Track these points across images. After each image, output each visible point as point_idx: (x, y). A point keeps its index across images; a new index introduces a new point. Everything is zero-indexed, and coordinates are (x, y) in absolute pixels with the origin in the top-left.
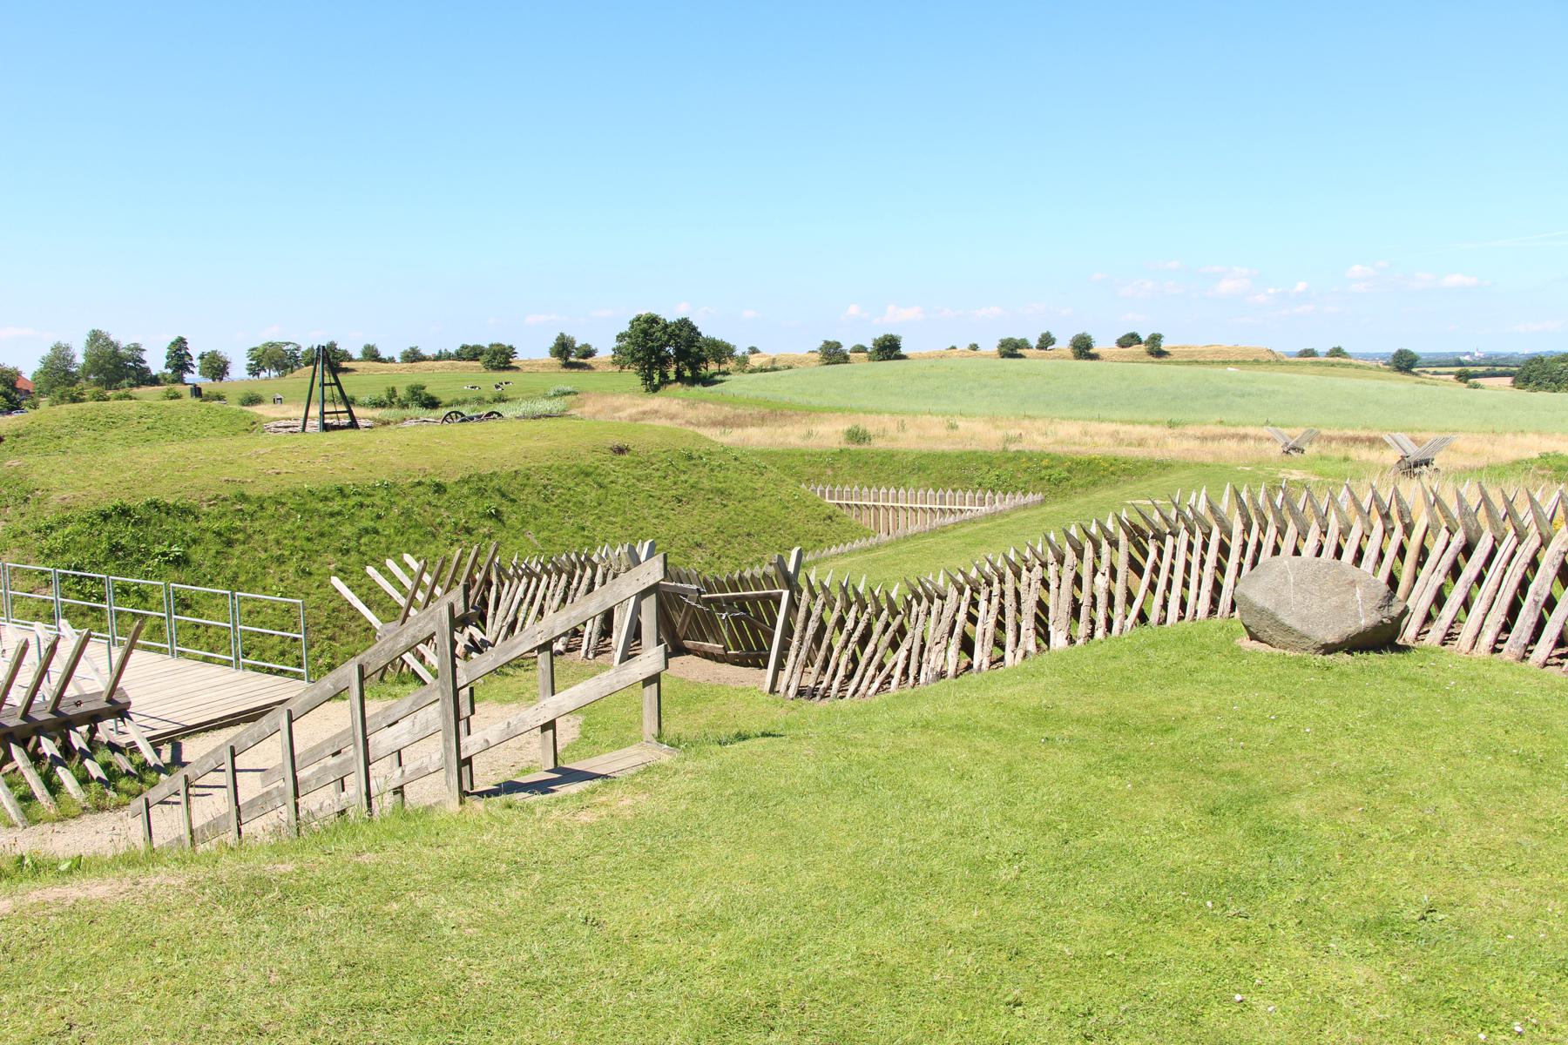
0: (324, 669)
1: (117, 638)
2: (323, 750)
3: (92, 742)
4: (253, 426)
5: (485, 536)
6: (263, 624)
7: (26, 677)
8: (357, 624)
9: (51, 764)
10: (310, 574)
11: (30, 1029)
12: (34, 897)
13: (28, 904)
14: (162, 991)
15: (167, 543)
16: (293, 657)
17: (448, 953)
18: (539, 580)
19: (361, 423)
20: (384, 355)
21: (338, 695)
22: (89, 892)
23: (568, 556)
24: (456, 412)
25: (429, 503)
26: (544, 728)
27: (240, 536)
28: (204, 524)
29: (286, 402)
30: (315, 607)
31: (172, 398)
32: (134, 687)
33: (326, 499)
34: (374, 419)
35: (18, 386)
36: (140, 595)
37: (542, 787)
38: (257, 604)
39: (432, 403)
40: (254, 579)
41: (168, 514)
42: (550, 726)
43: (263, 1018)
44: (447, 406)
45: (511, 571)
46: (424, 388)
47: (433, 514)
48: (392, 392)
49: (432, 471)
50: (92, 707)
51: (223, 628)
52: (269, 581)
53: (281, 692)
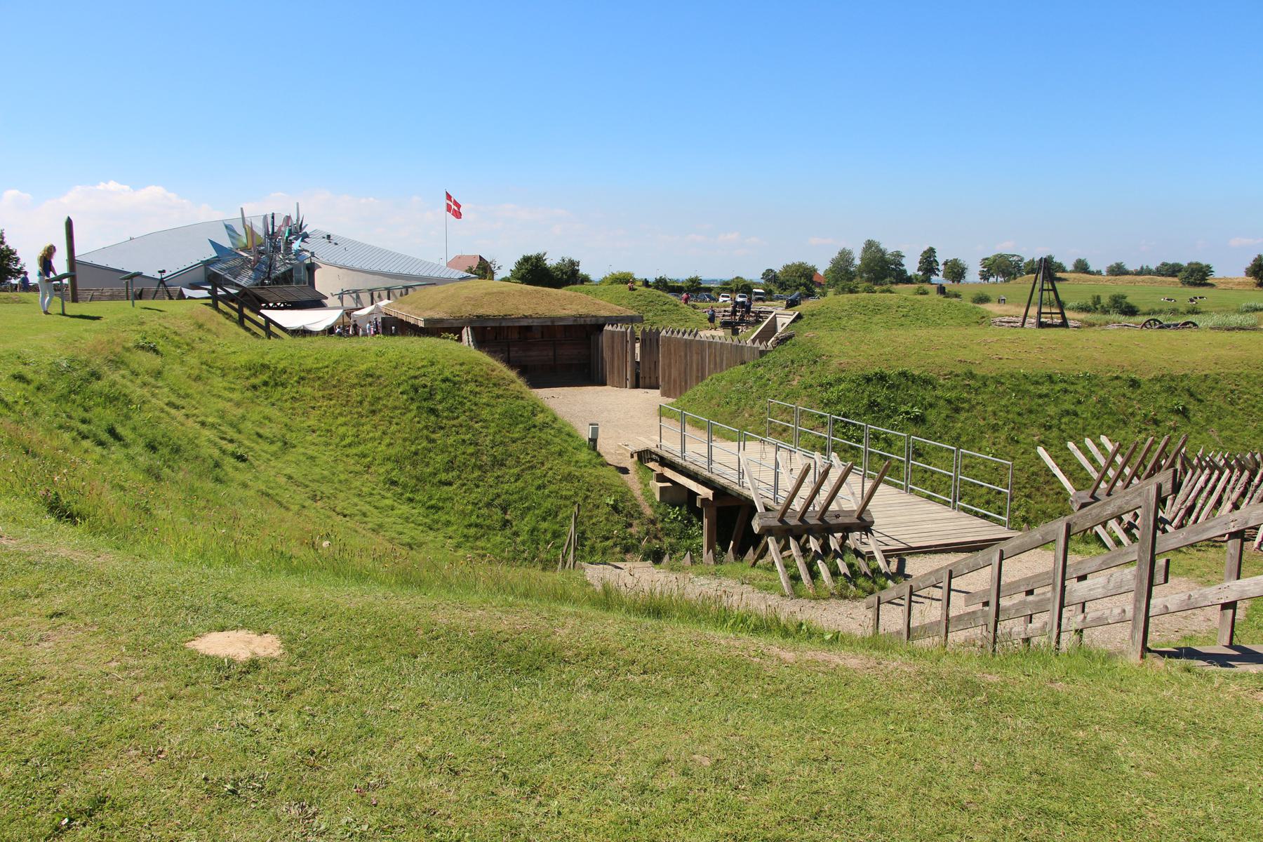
0: (1019, 520)
1: (868, 471)
2: (1019, 587)
3: (842, 546)
4: (983, 320)
5: (1170, 428)
6: (975, 477)
7: (805, 491)
8: (1051, 487)
9: (814, 556)
10: (1017, 442)
11: (801, 751)
12: (809, 655)
13: (805, 659)
14: (892, 752)
15: (910, 405)
16: (995, 506)
17: (1127, 789)
18: (1221, 473)
19: (1071, 323)
20: (1092, 268)
21: (1044, 544)
22: (846, 662)
23: (1253, 456)
24: (1155, 320)
25: (1124, 395)
26: (1225, 606)
27: (966, 405)
28: (939, 393)
29: (1009, 303)
30: (1019, 470)
31: (921, 294)
32: (876, 509)
33: (1037, 383)
34: (1081, 321)
35: (814, 280)
36: (887, 442)
37: (1222, 660)
38: (973, 460)
39: (1131, 311)
40: (973, 440)
41: (913, 382)
42: (1232, 605)
43: (966, 797)
44: (1144, 314)
45: (1195, 461)
46: (1125, 298)
47: (1126, 405)
48: (1097, 300)
49: (1130, 368)
50: (847, 521)
51: (945, 475)
52: (984, 443)
53: (985, 533)
